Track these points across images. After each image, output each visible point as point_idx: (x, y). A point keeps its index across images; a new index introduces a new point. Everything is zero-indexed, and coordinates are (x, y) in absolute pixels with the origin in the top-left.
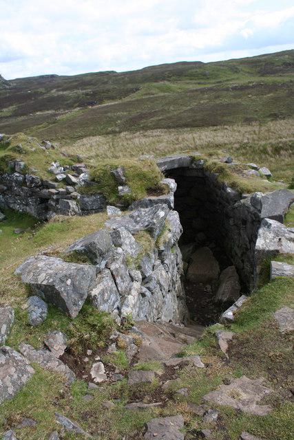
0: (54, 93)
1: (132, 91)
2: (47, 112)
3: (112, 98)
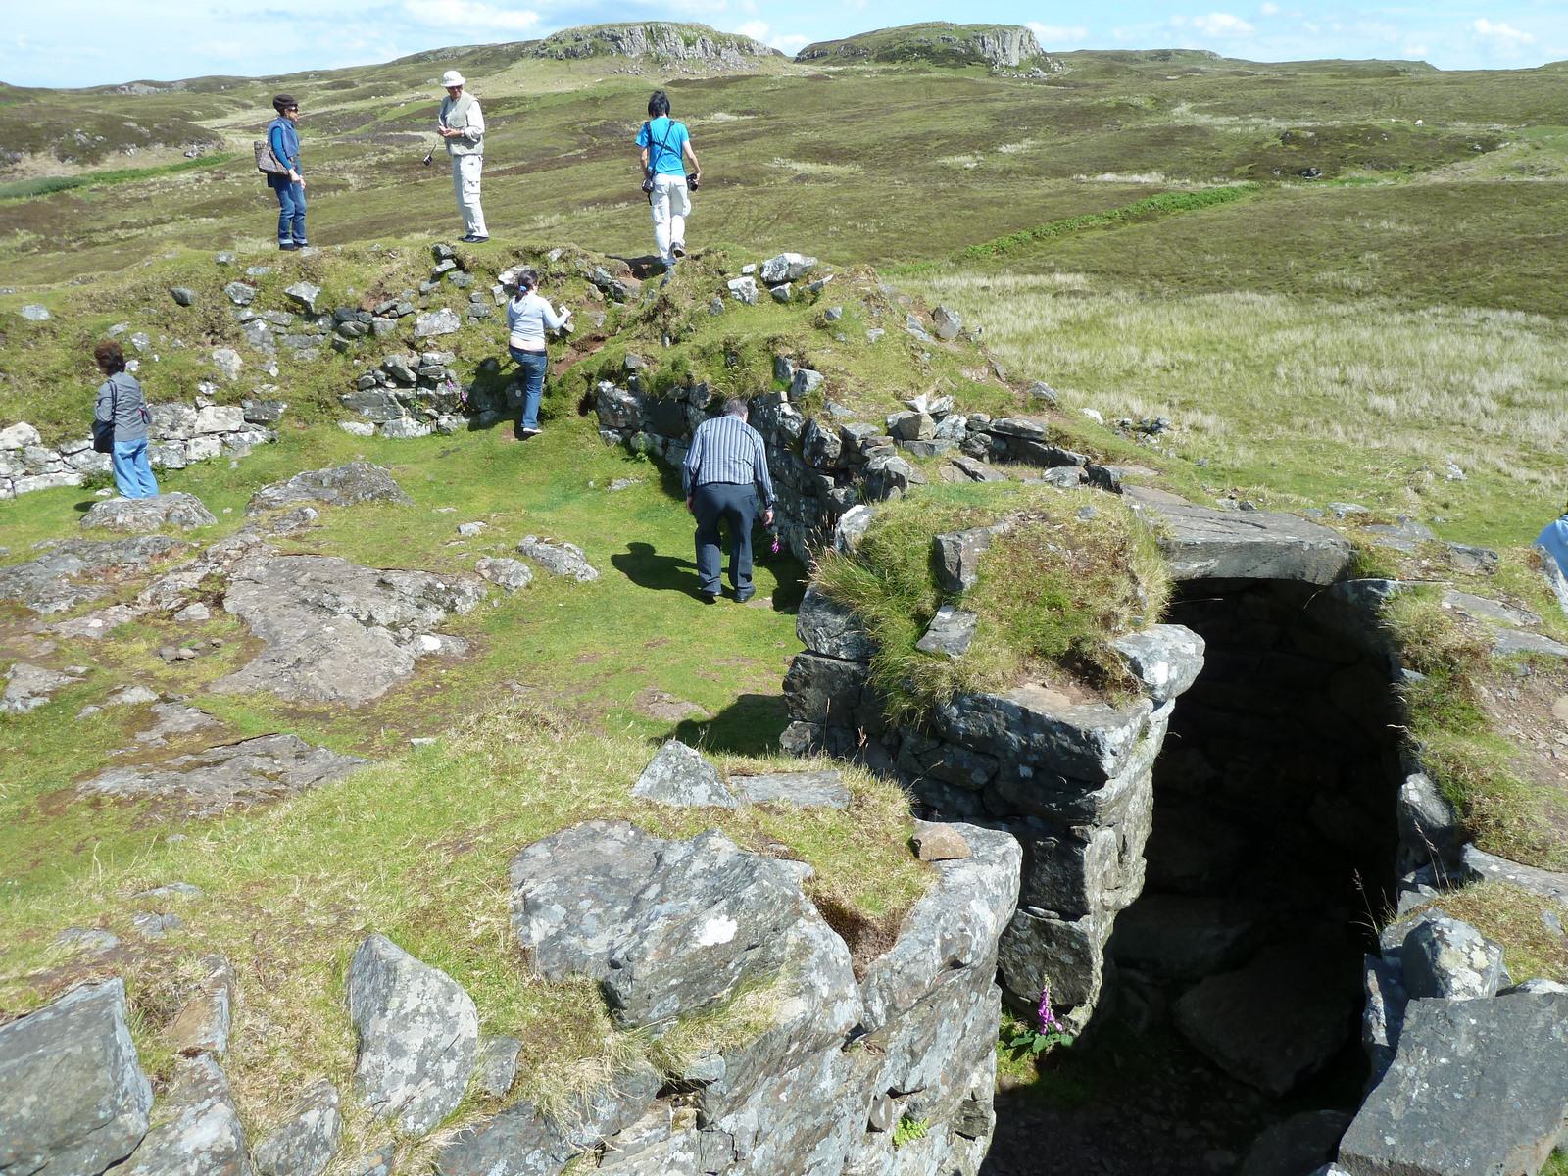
0: (1182, 113)
1: (1462, 149)
2: (1136, 178)
3: (1382, 165)
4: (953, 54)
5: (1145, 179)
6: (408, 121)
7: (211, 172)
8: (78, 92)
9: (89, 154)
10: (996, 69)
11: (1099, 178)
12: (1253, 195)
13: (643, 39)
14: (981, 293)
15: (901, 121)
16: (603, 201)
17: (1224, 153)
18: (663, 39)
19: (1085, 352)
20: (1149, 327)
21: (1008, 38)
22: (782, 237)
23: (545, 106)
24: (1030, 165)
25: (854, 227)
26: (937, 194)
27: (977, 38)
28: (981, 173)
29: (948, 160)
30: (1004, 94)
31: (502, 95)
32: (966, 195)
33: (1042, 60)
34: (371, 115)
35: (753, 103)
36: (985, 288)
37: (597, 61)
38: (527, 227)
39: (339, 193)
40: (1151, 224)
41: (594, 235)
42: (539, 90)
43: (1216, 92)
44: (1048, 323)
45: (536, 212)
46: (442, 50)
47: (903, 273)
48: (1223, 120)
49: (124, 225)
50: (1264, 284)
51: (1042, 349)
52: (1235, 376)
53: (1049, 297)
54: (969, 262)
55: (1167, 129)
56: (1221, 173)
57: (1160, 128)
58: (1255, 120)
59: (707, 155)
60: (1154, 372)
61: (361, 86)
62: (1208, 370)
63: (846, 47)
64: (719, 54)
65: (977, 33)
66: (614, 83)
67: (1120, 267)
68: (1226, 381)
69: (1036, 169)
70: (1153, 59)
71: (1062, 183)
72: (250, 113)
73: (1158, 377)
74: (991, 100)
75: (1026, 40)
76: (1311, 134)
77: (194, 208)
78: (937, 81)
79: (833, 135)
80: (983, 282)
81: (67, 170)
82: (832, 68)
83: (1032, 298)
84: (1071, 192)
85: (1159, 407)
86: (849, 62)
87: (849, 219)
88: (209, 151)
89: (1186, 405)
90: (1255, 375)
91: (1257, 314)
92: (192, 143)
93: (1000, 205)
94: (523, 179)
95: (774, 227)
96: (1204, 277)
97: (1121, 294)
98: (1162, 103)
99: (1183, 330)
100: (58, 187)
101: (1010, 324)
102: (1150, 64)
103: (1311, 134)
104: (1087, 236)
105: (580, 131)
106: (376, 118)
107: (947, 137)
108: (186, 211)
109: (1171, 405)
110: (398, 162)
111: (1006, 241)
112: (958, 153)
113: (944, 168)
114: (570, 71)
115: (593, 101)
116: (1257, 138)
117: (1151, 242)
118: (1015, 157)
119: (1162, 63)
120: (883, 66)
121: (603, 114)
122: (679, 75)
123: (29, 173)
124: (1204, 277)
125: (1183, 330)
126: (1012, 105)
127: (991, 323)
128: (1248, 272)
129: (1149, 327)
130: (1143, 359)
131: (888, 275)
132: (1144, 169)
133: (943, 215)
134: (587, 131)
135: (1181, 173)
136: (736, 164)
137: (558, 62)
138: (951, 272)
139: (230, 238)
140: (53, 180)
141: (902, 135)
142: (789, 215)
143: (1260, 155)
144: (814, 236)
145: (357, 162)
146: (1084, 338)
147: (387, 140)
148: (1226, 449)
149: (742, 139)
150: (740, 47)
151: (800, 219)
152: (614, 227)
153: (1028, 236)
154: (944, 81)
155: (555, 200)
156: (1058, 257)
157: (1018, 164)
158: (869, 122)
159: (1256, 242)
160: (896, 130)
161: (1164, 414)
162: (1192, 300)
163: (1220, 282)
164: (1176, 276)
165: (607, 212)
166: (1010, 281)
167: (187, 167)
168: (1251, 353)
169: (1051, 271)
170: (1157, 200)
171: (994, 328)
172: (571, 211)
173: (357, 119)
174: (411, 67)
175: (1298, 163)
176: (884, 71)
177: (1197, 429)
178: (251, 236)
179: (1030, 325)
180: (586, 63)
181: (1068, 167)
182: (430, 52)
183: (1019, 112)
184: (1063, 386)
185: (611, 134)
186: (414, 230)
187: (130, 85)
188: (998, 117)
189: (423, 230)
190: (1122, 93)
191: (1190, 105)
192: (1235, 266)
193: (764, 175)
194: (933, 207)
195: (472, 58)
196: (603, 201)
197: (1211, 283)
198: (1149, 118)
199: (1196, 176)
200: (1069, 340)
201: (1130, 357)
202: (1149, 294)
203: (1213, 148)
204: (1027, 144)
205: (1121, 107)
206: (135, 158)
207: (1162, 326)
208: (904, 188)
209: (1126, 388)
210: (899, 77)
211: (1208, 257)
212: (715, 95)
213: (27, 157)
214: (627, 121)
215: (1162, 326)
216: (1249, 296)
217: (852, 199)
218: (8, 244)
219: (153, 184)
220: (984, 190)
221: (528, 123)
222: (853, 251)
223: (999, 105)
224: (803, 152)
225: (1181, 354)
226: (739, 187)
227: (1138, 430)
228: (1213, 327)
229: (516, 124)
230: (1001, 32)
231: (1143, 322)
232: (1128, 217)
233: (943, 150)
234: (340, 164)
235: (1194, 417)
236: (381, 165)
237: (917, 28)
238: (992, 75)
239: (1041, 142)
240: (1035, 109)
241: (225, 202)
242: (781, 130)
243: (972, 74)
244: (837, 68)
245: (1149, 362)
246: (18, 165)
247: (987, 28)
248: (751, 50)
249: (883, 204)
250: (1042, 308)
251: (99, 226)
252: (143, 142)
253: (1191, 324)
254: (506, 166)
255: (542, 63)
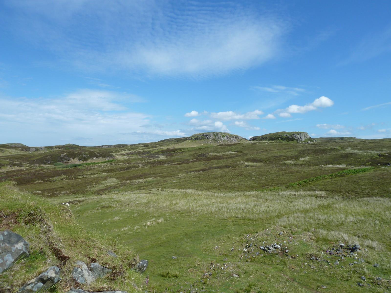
2: (338, 166)
4: (288, 138)
5: (340, 166)
6: (157, 153)
7: (110, 163)
8: (92, 147)
9: (85, 159)
10: (299, 141)
11: (327, 166)
12: (373, 170)
13: (213, 136)
14: (293, 196)
15: (274, 153)
16: (196, 171)
17: (362, 159)
18: (217, 136)
19: (326, 216)
20: (347, 208)
21: (301, 135)
22: (239, 180)
23: (189, 150)
24: (308, 163)
25: (259, 178)
26: (282, 170)
27: (293, 135)
28: (294, 165)
29: (286, 162)
30: (301, 147)
31: (179, 148)
32: (290, 170)
33: (310, 139)
34: (150, 152)
35: (238, 149)
36: (295, 195)
37: (202, 140)
38: (176, 177)
39: (137, 168)
40: (344, 178)
41: (191, 179)
42: (188, 147)
43: (358, 145)
44: (314, 206)
45: (179, 173)
46: (170, 139)
47: (271, 190)
48: (360, 152)
49: (87, 175)
50: (383, 195)
51: (311, 214)
52: (380, 226)
53: (314, 198)
54: (290, 187)
55: (345, 154)
56: (362, 165)
57: (343, 154)
58: (370, 151)
59: (224, 161)
60: (351, 224)
61: (150, 146)
62: (370, 224)
63: (261, 137)
64: (231, 139)
65: (293, 134)
66: (206, 145)
67: (335, 189)
68: (377, 228)
69: (309, 164)
70: (339, 139)
71: (317, 167)
72: (125, 152)
73: (352, 226)
74: (297, 148)
75: (306, 135)
76: (387, 154)
77: (103, 171)
78: (284, 144)
79: (256, 156)
80: (294, 193)
81: (80, 162)
82: (258, 142)
83: (309, 198)
84: (319, 169)
85: (354, 238)
86: (262, 141)
87: (258, 176)
88: (111, 159)
89: (365, 237)
90: (387, 226)
91: (382, 204)
92: (108, 157)
93: (299, 172)
94: (179, 166)
95: (238, 178)
96: (363, 192)
97: (337, 197)
98: (343, 148)
99: (358, 209)
100: (75, 166)
101: (302, 206)
102: (339, 140)
103: (387, 154)
104: (325, 181)
105: (196, 155)
106: (150, 152)
107: (285, 156)
108: (101, 172)
109: (358, 237)
110: (152, 162)
111: (301, 182)
112: (288, 160)
113: (285, 163)
114: (196, 143)
115: (200, 149)
116: (372, 156)
117: (345, 183)
118: (304, 161)
119: (342, 140)
120: (270, 141)
121: (202, 152)
122: (221, 143)
123: (72, 163)
124: (363, 192)
125: (358, 209)
126: (303, 149)
127: (295, 205)
128: (376, 191)
129: (347, 208)
130: (346, 219)
131: (266, 191)
132: (340, 164)
133: (283, 175)
134: (197, 155)
135: (351, 165)
136: (231, 163)
137: (193, 141)
138: (285, 190)
139: (107, 178)
140: (75, 164)
141: (274, 156)
142: (242, 175)
143: (373, 160)
144: (248, 180)
145: (143, 162)
146: (325, 211)
147: (151, 157)
148: (385, 259)
149: (233, 157)
150: (236, 137)
151: (244, 176)
152: (196, 177)
153: (308, 181)
154: (285, 144)
155: (184, 171)
156: (316, 186)
157: (304, 163)
158: (266, 153)
159: (377, 183)
160: (272, 155)
161: (357, 242)
162: (360, 200)
163: (368, 194)
164: (354, 192)
165: (196, 174)
166: (302, 193)
167: (106, 162)
168: (384, 217)
169: (315, 190)
170: (345, 171)
171: (296, 207)
172: (188, 173)
173: (146, 153)
174: (162, 142)
175: (385, 162)
176: (270, 142)
177: (370, 247)
178: (112, 178)
179: (308, 206)
180: (200, 141)
181: (318, 163)
182: (167, 139)
183: (305, 150)
184: (319, 228)
185: (203, 156)
186: (149, 177)
187: (103, 146)
188: (299, 152)
189: (151, 177)
190: (332, 146)
191: (351, 148)
192: (372, 189)
193: (237, 165)
194: (281, 173)
195: (175, 140)
196: (196, 171)
197: (365, 194)
198: (340, 151)
199: (355, 165)
200: (321, 212)
201: (341, 218)
202: (346, 198)
203: (359, 158)
204: (307, 158)
205: (332, 149)
206: (95, 160)
207: (351, 208)
208: (273, 168)
209: (341, 229)
210: (274, 144)
211: (363, 187)
212: (229, 148)
213: (72, 159)
214: (207, 153)
215: (351, 208)
216: (378, 198)
217: (259, 171)
218: (59, 178)
219: (96, 166)
220: (295, 169)
221: (184, 154)
222: (258, 184)
223: (299, 149)
224: (248, 160)
225: (359, 217)
226: (231, 168)
227: (347, 249)
228: (369, 209)
229: (181, 154)
230: (299, 133)
231: (345, 206)
232: (336, 176)
233: (285, 159)
234: (139, 162)
235: (368, 242)
236: (148, 163)
237: (279, 133)
238: (298, 143)
239: (311, 157)
240: (309, 150)
241: (110, 170)
242: (244, 155)
243: (293, 143)
244: (259, 142)
245: (348, 220)
246: (70, 161)
247: (296, 132)
248: (238, 138)
249: (267, 172)
250: (312, 201)
251: (81, 174)
252: (97, 157)
253: (361, 207)
254: (177, 163)
255: (189, 141)
